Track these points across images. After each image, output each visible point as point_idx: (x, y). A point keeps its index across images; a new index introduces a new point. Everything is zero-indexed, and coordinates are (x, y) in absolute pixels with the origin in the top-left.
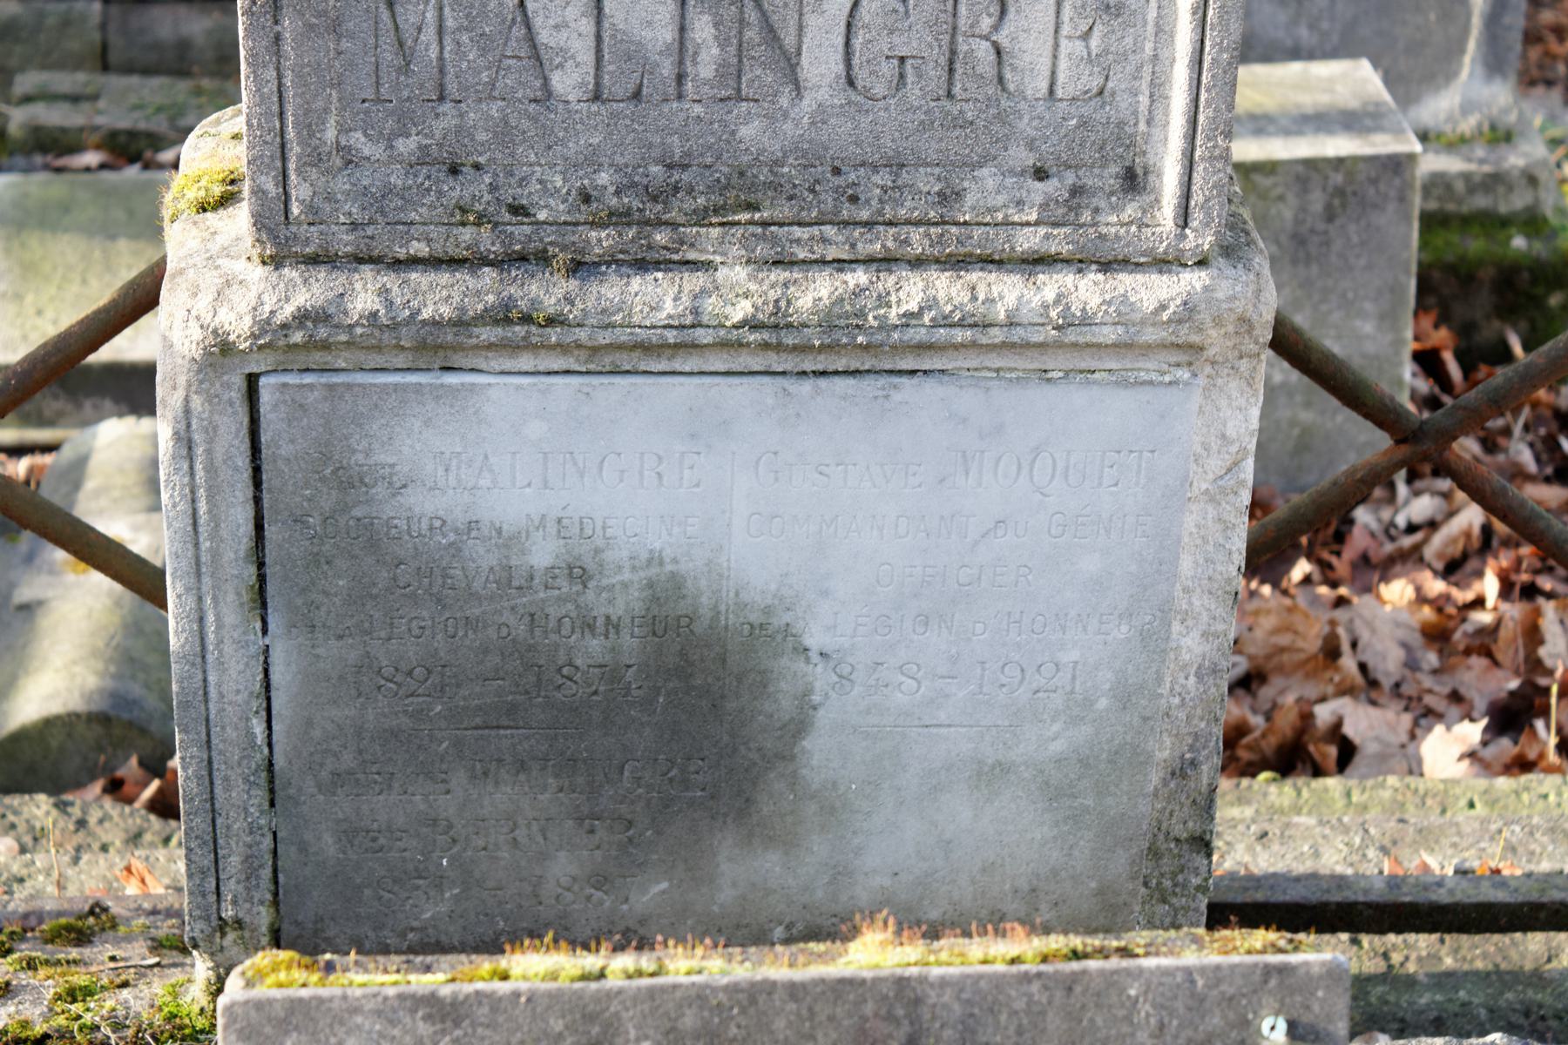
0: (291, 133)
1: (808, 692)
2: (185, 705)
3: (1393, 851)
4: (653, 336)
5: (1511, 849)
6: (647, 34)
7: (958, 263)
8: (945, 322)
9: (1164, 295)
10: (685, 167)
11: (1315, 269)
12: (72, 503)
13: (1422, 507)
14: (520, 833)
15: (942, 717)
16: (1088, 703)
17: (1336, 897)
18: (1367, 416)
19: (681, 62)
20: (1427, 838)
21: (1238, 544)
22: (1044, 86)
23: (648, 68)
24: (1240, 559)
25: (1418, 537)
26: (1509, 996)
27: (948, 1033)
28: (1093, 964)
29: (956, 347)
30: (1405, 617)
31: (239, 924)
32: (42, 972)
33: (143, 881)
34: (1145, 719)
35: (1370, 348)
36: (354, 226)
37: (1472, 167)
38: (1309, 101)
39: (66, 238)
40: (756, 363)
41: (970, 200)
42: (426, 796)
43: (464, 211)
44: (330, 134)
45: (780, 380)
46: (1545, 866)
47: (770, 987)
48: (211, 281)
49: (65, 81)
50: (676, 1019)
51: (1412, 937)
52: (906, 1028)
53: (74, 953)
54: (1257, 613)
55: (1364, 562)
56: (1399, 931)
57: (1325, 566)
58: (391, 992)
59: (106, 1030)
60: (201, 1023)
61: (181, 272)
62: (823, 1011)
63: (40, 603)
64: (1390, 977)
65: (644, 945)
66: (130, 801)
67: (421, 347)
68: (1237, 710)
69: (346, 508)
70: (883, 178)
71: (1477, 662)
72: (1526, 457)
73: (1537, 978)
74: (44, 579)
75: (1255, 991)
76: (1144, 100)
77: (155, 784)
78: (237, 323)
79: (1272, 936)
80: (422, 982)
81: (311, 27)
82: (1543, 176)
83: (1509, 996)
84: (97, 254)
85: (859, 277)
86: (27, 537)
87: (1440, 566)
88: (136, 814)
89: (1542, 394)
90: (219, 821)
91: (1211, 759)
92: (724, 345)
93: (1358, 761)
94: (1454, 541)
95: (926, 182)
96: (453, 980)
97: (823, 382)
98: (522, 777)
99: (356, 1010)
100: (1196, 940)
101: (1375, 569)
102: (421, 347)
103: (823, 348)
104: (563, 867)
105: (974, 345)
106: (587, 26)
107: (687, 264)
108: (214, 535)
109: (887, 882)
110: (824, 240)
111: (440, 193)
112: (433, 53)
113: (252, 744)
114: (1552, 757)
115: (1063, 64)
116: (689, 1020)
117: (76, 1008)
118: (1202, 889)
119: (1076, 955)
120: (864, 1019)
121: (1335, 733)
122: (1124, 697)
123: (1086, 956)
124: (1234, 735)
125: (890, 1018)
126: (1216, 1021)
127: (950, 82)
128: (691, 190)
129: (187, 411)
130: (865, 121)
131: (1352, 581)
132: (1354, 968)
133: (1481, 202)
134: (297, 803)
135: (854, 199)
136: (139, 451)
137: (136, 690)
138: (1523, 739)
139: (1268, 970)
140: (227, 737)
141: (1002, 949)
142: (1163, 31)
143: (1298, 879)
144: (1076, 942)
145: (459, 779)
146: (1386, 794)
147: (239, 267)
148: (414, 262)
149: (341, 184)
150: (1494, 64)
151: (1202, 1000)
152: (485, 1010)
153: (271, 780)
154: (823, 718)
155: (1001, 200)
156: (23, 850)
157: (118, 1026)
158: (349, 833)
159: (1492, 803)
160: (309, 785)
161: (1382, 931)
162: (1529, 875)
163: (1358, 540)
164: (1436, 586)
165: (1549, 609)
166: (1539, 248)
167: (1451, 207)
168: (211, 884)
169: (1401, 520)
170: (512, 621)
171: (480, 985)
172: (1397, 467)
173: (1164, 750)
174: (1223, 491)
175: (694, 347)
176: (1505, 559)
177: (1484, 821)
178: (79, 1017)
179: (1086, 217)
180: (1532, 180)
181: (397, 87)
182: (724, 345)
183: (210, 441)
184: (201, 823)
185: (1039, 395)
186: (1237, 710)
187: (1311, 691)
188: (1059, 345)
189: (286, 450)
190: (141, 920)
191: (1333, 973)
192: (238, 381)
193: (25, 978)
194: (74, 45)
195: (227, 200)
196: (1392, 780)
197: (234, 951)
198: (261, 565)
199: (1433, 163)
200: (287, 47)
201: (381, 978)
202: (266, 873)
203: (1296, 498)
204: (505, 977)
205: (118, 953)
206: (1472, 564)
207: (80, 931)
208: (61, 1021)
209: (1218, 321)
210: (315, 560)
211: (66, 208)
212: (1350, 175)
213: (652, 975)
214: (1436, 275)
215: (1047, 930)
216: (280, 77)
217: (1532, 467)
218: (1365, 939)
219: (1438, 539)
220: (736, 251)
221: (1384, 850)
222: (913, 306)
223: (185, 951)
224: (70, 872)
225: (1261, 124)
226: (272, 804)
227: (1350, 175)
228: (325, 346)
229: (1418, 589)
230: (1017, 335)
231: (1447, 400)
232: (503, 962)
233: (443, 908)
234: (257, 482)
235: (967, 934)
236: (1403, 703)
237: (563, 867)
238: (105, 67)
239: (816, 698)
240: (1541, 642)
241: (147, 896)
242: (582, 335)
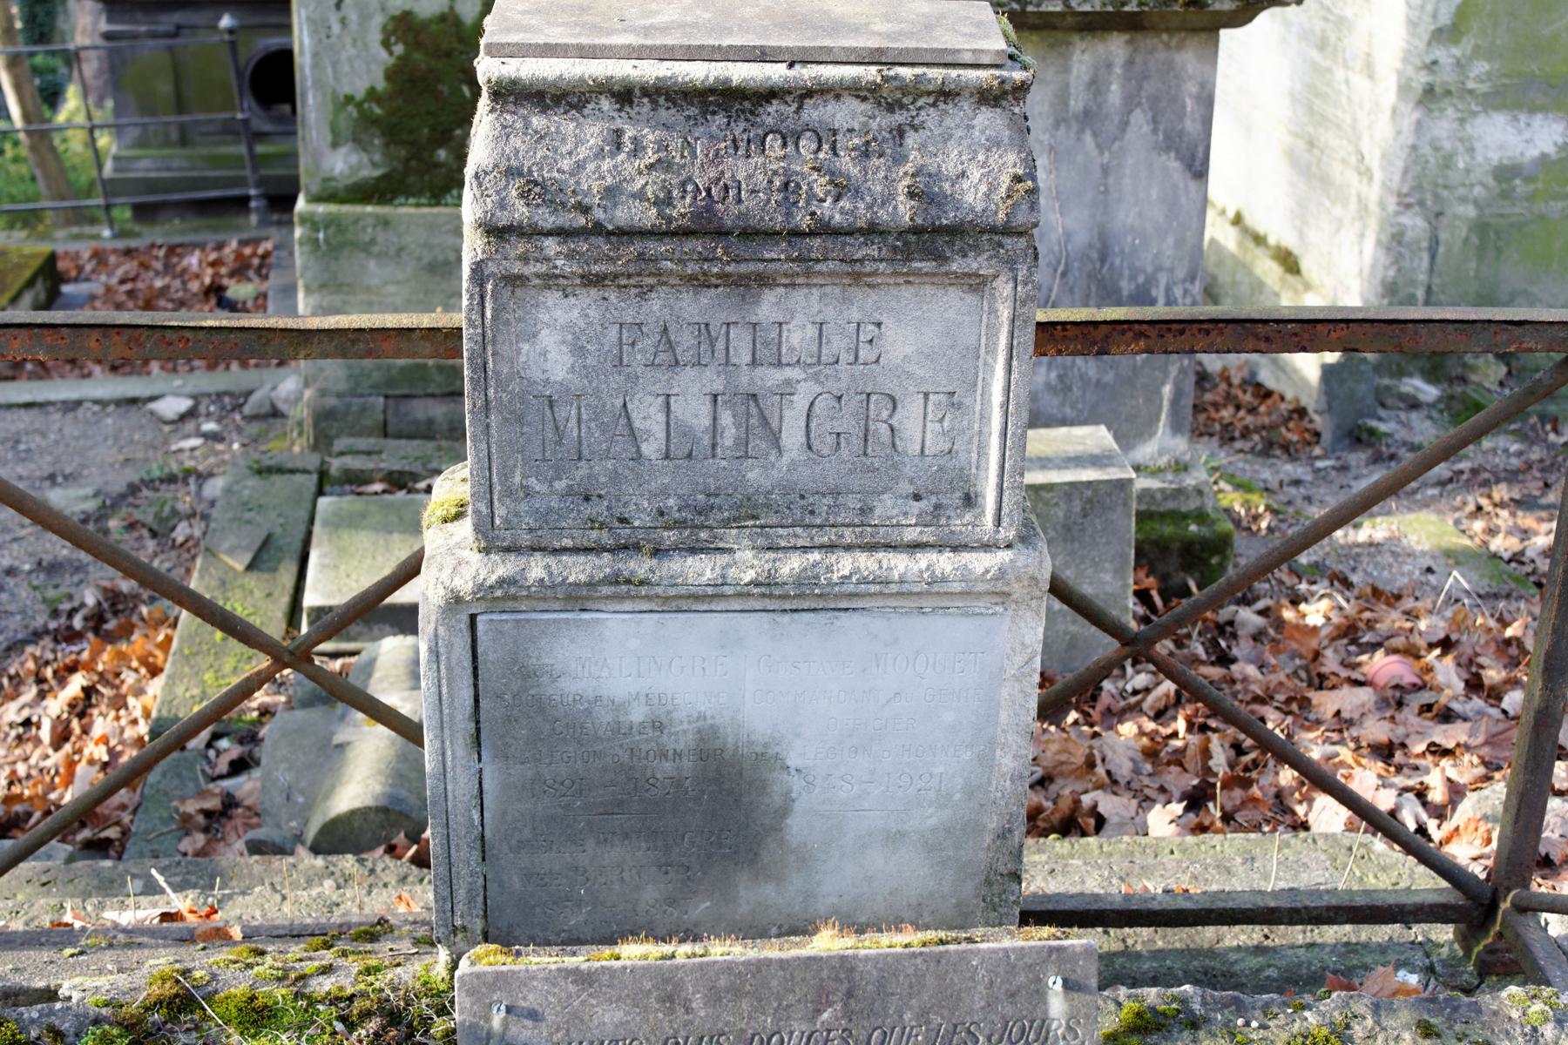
0: (495, 479)
1: (789, 791)
2: (434, 803)
4: (700, 591)
5: (1195, 877)
6: (695, 421)
7: (872, 547)
8: (864, 581)
9: (987, 565)
10: (717, 495)
11: (1076, 545)
12: (367, 686)
13: (1141, 680)
14: (626, 875)
15: (866, 805)
16: (949, 796)
17: (1094, 907)
18: (1105, 630)
19: (714, 437)
20: (1146, 871)
21: (1033, 705)
22: (918, 448)
23: (696, 440)
24: (1034, 713)
25: (1139, 697)
26: (1195, 963)
27: (870, 987)
28: (951, 947)
29: (871, 595)
30: (1132, 743)
31: (464, 929)
32: (351, 958)
35: (1109, 589)
36: (531, 530)
37: (1165, 485)
38: (1072, 449)
39: (364, 533)
40: (758, 605)
41: (877, 512)
43: (592, 521)
44: (517, 479)
45: (771, 615)
46: (1214, 888)
47: (768, 962)
48: (450, 562)
49: (363, 443)
51: (1139, 930)
52: (846, 985)
53: (369, 947)
54: (1047, 742)
55: (1109, 711)
56: (1131, 926)
57: (1086, 714)
58: (553, 967)
59: (388, 991)
60: (442, 987)
61: (433, 557)
62: (799, 976)
63: (348, 743)
64: (1127, 953)
65: (696, 939)
66: (400, 858)
67: (568, 598)
68: (1037, 798)
69: (526, 690)
70: (828, 500)
71: (1174, 769)
72: (1200, 651)
73: (1211, 953)
74: (351, 729)
76: (974, 455)
77: (415, 848)
78: (465, 585)
79: (1053, 930)
80: (571, 962)
81: (507, 420)
82: (1206, 490)
83: (1195, 963)
84: (381, 542)
85: (815, 556)
86: (340, 706)
87: (1152, 714)
88: (404, 866)
89: (1209, 614)
91: (1020, 827)
92: (739, 595)
94: (1160, 699)
95: (853, 502)
97: (796, 616)
99: (534, 978)
100: (1010, 933)
101: (1114, 716)
102: (568, 598)
103: (796, 596)
104: (650, 894)
105: (881, 593)
106: (661, 417)
107: (722, 550)
108: (451, 705)
109: (835, 900)
110: (796, 536)
111: (579, 512)
112: (575, 434)
114: (1219, 824)
115: (929, 436)
116: (723, 982)
117: (371, 979)
118: (1016, 903)
119: (942, 942)
120: (822, 980)
121: (1094, 811)
122: (970, 792)
123: (948, 943)
124: (1034, 814)
125: (837, 979)
126: (1022, 979)
127: (865, 446)
128: (720, 509)
129: (436, 635)
130: (818, 469)
131: (1102, 723)
132: (1106, 948)
133: (1171, 505)
135: (812, 512)
136: (406, 655)
137: (404, 793)
138: (1201, 813)
139: (1051, 950)
140: (459, 820)
141: (900, 939)
142: (985, 418)
143: (1072, 896)
144: (942, 934)
145: (590, 843)
146: (1123, 846)
147: (466, 554)
148: (564, 550)
149: (523, 507)
150: (1176, 428)
151: (1014, 967)
153: (483, 846)
154: (798, 807)
155: (895, 512)
156: (339, 887)
157: (395, 989)
158: (527, 876)
159: (1184, 851)
161: (1121, 926)
162: (1205, 893)
163: (1105, 700)
164: (1150, 726)
165: (1215, 737)
166: (1205, 531)
167: (1154, 508)
169: (1129, 688)
170: (621, 753)
171: (604, 963)
172: (1126, 658)
173: (993, 823)
174: (1023, 674)
175: (723, 596)
176: (1189, 710)
177: (1179, 862)
179: (943, 521)
180: (1199, 492)
181: (555, 452)
182: (739, 595)
183: (449, 652)
184: (443, 870)
185: (918, 622)
186: (1037, 798)
187: (1079, 787)
188: (929, 593)
189: (492, 657)
190: (408, 927)
191: (1088, 951)
192: (465, 618)
193: (340, 961)
194: (368, 422)
195: (458, 516)
196: (1126, 838)
197: (462, 945)
198: (478, 722)
199: (1142, 483)
200: (493, 431)
201: (547, 959)
202: (480, 899)
203: (1069, 676)
204: (618, 958)
206: (1170, 713)
207: (372, 934)
208: (362, 986)
209: (1018, 579)
210: (508, 719)
211: (363, 515)
212: (1095, 491)
214: (1146, 547)
215: (927, 927)
216: (489, 448)
217: (1204, 657)
218: (1112, 931)
219: (1150, 699)
220: (746, 542)
221: (1122, 879)
222: (846, 572)
223: (433, 945)
224: (366, 900)
225: (1044, 463)
227: (1095, 491)
228: (515, 598)
229: (1140, 727)
230: (905, 588)
231: (1153, 617)
232: (616, 950)
233: (581, 919)
234: (476, 675)
235: (880, 930)
236: (1506, 661)
237: (650, 894)
238: (386, 435)
239: (794, 795)
240: (1211, 758)
241: (411, 913)
242: (659, 590)
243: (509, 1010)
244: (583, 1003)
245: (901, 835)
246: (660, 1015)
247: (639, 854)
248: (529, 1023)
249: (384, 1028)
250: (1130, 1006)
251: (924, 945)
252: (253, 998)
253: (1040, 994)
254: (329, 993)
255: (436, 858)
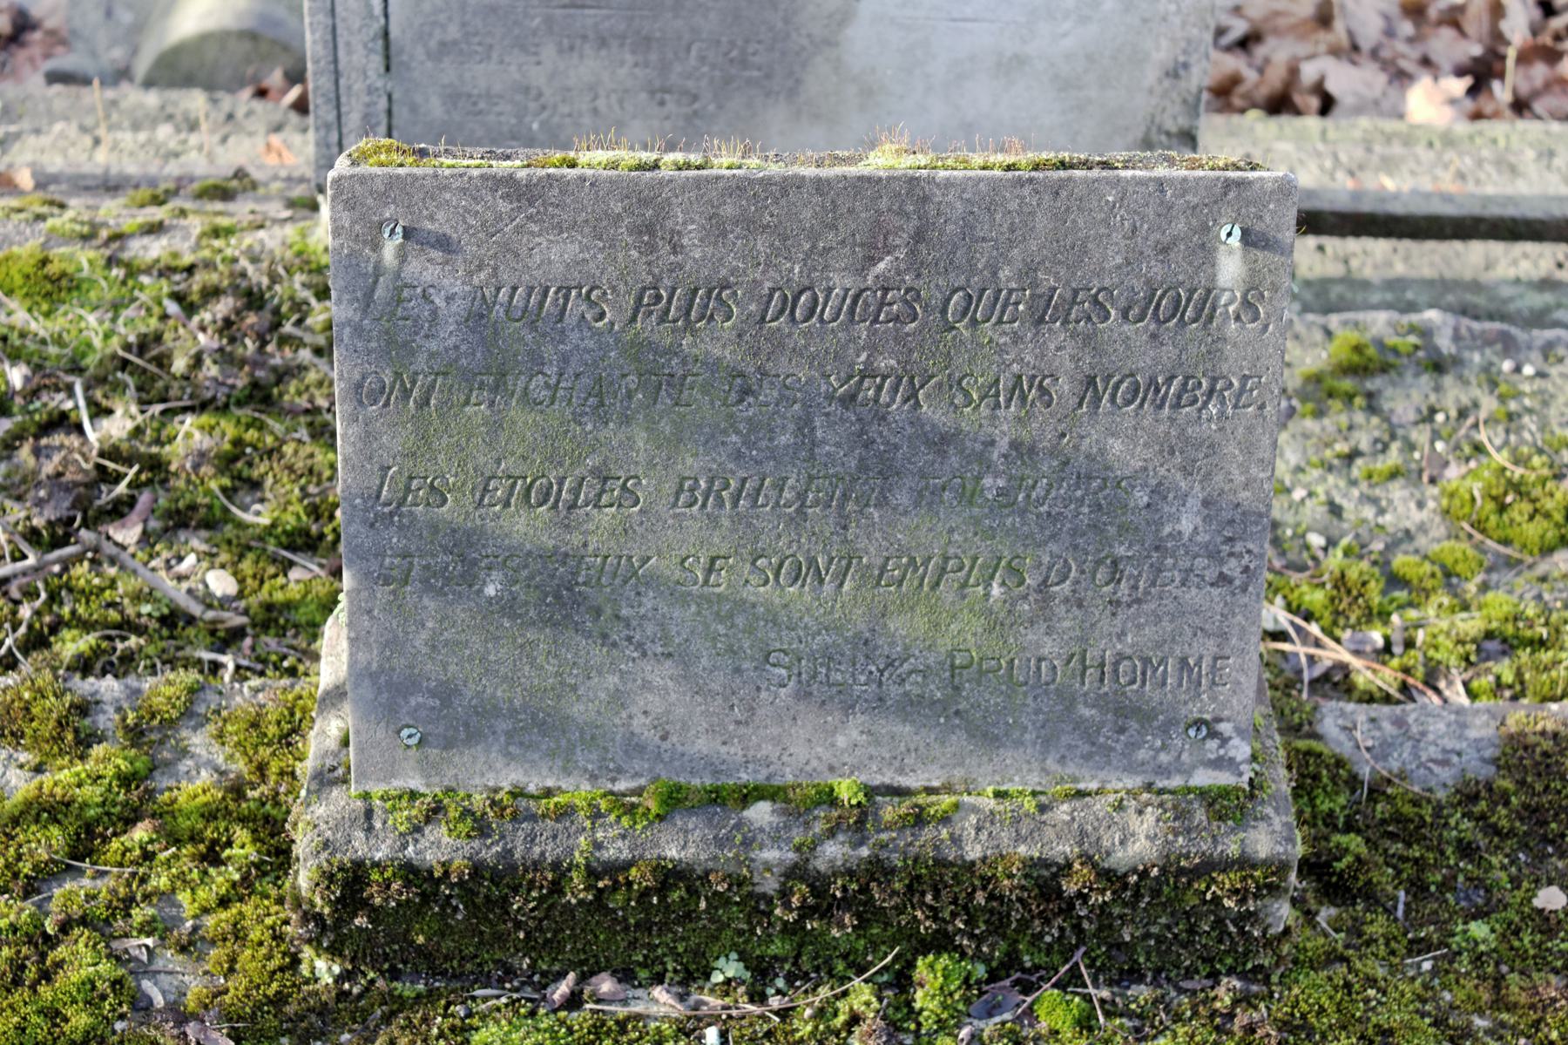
3: (1358, 174)
20: (1389, 165)
27: (950, 228)
28: (1078, 173)
33: (280, 155)
34: (1145, 21)
42: (520, 66)
47: (799, 182)
50: (718, 207)
52: (915, 222)
58: (476, 173)
59: (244, 263)
71: (1447, 33)
75: (1216, 202)
80: (502, 167)
90: (342, 82)
93: (1336, 112)
96: (529, 166)
98: (603, 53)
113: (371, 16)
117: (217, 243)
123: (1072, 167)
126: (1180, 226)
134: (408, 68)
139: (1228, 185)
145: (549, 52)
152: (556, 191)
153: (387, 46)
157: (255, 260)
158: (453, 97)
160: (420, 52)
168: (334, 137)
171: (551, 170)
173: (1162, 53)
178: (220, 251)
187: (1302, 49)
204: (573, 165)
205: (258, 208)
208: (206, 253)
213: (698, 168)
226: (388, 69)
241: (282, 166)
243: (408, 234)
244: (518, 230)
245: (1020, 61)
246: (634, 253)
247: (623, 72)
248: (437, 255)
249: (238, 312)
250: (1346, 338)
251: (1036, 167)
252: (44, 262)
253: (1206, 252)
254: (157, 261)
255: (316, 62)
